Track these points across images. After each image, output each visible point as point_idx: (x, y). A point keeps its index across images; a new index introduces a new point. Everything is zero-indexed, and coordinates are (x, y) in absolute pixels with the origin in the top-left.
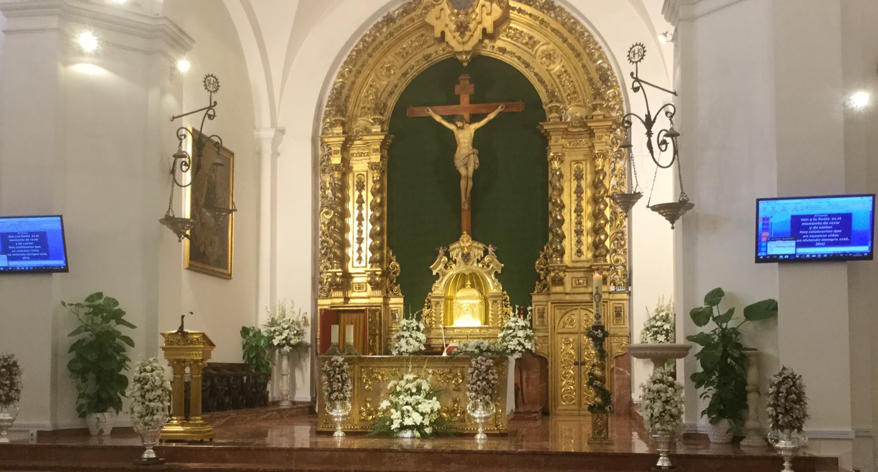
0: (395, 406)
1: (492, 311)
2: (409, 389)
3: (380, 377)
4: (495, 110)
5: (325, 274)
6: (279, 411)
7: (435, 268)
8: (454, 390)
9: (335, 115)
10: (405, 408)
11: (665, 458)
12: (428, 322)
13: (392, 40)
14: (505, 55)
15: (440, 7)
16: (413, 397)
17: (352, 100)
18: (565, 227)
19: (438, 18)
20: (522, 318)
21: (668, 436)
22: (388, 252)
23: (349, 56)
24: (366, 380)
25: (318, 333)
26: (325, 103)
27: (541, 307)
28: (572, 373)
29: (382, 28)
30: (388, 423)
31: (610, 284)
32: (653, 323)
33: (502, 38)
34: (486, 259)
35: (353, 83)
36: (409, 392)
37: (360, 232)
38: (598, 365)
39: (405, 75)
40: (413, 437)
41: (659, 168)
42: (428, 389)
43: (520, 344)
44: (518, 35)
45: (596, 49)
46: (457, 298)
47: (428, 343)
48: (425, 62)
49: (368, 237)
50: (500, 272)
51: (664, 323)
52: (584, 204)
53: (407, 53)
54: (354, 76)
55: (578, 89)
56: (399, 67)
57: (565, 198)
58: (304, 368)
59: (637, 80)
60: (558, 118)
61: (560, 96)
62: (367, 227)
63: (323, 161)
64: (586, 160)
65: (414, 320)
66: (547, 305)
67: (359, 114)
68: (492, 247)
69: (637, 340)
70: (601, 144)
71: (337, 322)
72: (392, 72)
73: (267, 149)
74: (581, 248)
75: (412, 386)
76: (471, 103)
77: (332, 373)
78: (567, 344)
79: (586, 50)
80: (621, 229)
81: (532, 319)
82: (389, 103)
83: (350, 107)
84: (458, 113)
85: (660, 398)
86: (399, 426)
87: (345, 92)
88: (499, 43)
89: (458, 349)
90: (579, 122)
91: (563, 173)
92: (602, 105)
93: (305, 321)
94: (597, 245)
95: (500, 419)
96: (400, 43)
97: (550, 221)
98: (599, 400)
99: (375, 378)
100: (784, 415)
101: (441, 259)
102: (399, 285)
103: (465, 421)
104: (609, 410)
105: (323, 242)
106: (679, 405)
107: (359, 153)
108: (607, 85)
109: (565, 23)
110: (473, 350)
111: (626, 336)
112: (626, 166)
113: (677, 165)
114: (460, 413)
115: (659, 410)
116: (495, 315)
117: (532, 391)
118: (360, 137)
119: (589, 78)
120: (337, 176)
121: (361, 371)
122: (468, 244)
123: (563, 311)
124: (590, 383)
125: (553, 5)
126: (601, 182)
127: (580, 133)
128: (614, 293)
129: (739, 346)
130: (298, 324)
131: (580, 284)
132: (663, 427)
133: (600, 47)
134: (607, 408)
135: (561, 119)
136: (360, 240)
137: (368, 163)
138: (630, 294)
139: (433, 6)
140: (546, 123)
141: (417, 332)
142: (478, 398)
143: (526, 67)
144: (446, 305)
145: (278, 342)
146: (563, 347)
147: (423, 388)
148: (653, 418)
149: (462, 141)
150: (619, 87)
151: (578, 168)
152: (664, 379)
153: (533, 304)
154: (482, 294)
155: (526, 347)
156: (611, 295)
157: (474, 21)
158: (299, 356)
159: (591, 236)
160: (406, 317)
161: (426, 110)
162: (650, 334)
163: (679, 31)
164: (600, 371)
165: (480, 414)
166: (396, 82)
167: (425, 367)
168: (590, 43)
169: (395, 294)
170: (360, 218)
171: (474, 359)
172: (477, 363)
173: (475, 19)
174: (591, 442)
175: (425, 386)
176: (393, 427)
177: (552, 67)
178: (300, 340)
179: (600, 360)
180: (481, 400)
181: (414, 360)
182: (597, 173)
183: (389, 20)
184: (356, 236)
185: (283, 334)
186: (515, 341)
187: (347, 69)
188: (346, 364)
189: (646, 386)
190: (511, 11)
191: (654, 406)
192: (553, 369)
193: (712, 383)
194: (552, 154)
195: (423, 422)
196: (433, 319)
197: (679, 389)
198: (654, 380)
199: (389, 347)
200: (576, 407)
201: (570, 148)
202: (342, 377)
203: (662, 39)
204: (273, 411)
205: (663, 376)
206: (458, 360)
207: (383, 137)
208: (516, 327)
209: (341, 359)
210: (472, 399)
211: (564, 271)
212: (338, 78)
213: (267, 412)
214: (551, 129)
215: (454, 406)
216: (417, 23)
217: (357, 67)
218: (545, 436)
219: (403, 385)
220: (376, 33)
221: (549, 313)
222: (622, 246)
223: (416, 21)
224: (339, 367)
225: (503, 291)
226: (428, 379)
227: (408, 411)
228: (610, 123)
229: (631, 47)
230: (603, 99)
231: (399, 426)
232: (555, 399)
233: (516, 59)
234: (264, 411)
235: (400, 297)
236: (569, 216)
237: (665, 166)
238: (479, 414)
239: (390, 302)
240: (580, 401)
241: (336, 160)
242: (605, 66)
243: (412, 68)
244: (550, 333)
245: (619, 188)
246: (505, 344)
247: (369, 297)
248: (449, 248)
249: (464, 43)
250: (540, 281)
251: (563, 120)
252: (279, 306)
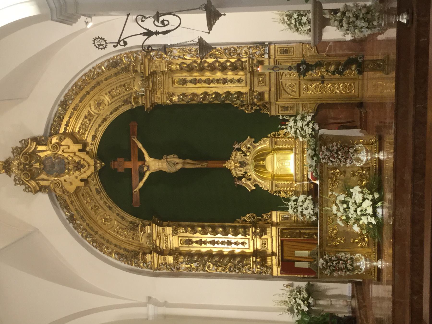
0: (357, 220)
1: (282, 145)
2: (344, 209)
3: (335, 231)
4: (136, 144)
5: (254, 270)
6: (360, 308)
7: (250, 188)
8: (345, 175)
9: (138, 259)
10: (359, 213)
11: (400, 17)
12: (291, 193)
13: (86, 217)
14: (97, 135)
15: (63, 182)
16: (350, 206)
17: (127, 247)
18: (221, 91)
19: (71, 184)
20: (288, 123)
21: (383, 15)
22: (238, 223)
23: (96, 248)
24: (337, 242)
25: (299, 276)
26: (130, 266)
27: (280, 109)
28: (330, 85)
29: (77, 224)
30: (371, 226)
31: (263, 58)
32: (292, 26)
33: (86, 138)
34: (244, 149)
35: (116, 246)
36: (346, 209)
37: (223, 243)
38: (327, 68)
39: (110, 208)
40: (382, 207)
41: (180, 26)
42: (344, 195)
43: (308, 125)
44: (84, 127)
45: (95, 70)
46: (273, 171)
47: (307, 194)
48: (101, 193)
49: (227, 237)
50: (253, 140)
51: (293, 18)
52: (203, 78)
53: (95, 206)
54: (111, 245)
55: (122, 83)
56: (105, 212)
57: (199, 91)
58: (326, 287)
59: (118, 43)
60: (142, 97)
61: (127, 96)
62: (219, 237)
63: (171, 269)
64: (172, 77)
65: (289, 204)
66: (278, 105)
67: (138, 242)
68: (235, 145)
69: (308, 38)
70: (161, 66)
71: (293, 262)
72: (108, 217)
73: (162, 310)
74: (236, 79)
75: (342, 207)
76: (130, 160)
77: (332, 268)
78: (307, 89)
79: (95, 77)
80: (222, 51)
81: (288, 116)
82: (130, 220)
83: (132, 248)
84: (138, 170)
85: (354, 22)
86: (374, 218)
87: (122, 252)
88: (89, 140)
89: (313, 172)
90: (145, 82)
91: (181, 93)
92: (133, 66)
93: (289, 286)
94: (235, 68)
95: (368, 141)
96: (88, 212)
97: (216, 102)
98: (354, 67)
99: (335, 235)
101: (243, 183)
102: (263, 214)
103: (369, 168)
104: (362, 59)
105: (230, 271)
106: (360, 7)
107: (165, 243)
108: (120, 62)
109: (76, 92)
110: (314, 161)
111: (302, 46)
112: (177, 48)
113: (178, 12)
114: (363, 171)
115: (363, 23)
116: (286, 143)
117: (343, 116)
118: (154, 241)
119: (114, 76)
120: (182, 259)
121: (330, 246)
122: (233, 163)
123: (283, 92)
125: (63, 101)
126: (188, 66)
127: (153, 82)
128: (270, 55)
130: (292, 291)
131: (262, 80)
132: (376, 19)
133: (93, 68)
134: (360, 60)
135: (143, 95)
136: (229, 243)
137: (173, 236)
138: (270, 43)
139: (62, 187)
140: (146, 106)
141: (298, 201)
142: (352, 158)
143: (106, 121)
144: (278, 180)
145: (306, 307)
146: (310, 92)
147: (343, 199)
148: (369, 27)
150: (121, 54)
151: (178, 82)
152: (339, 19)
153: (278, 114)
154: (269, 153)
155: (310, 120)
156: (271, 57)
157: (74, 158)
158: (317, 291)
159: (228, 72)
160: (287, 209)
161: (135, 193)
162: (301, 27)
163: (84, 13)
164: (331, 66)
165: (363, 156)
166: (115, 214)
167: (327, 197)
168: (90, 75)
169: (270, 218)
170: (213, 243)
171: (321, 160)
172: (324, 158)
173: (72, 157)
174: (386, 73)
175: (342, 197)
176: (374, 222)
177: (106, 102)
178: (304, 290)
179: (323, 66)
180: (353, 155)
181: (322, 205)
182: (182, 69)
183: (72, 219)
184: (226, 246)
185: (299, 303)
186: (306, 128)
187: (106, 250)
188: (324, 257)
189: (345, 32)
190: (67, 132)
191: (360, 26)
192: (327, 100)
194: (168, 102)
195: (370, 199)
196: (288, 189)
197: (347, 8)
198: (339, 27)
199: (310, 223)
200: (357, 83)
201: (164, 89)
202: (335, 261)
203: (90, 25)
204: (360, 313)
205: (337, 20)
206: (322, 172)
207: (154, 225)
208: (295, 127)
209: (321, 261)
210: (352, 162)
211: (253, 92)
212: (112, 257)
213: (361, 318)
214: (150, 102)
215: (358, 176)
216: (74, 198)
217: (104, 242)
218: (381, 105)
219: (341, 214)
220: (80, 228)
221: (285, 103)
222: (235, 49)
223: (73, 200)
224: (327, 263)
225: (267, 137)
226: (336, 195)
227: (362, 211)
228: (146, 60)
229: (95, 47)
230: (129, 65)
231: (374, 218)
232: (350, 98)
233: (100, 128)
234: (360, 320)
235: (272, 214)
236: (213, 89)
237: (179, 19)
238: (364, 157)
239: (275, 221)
240: (352, 79)
241: (170, 259)
242: (106, 64)
243: (105, 203)
244: (299, 102)
245: (193, 53)
246: (307, 136)
247: (272, 237)
248: (235, 177)
249: (89, 165)
250: (261, 109)
251: (144, 94)
252: (278, 305)
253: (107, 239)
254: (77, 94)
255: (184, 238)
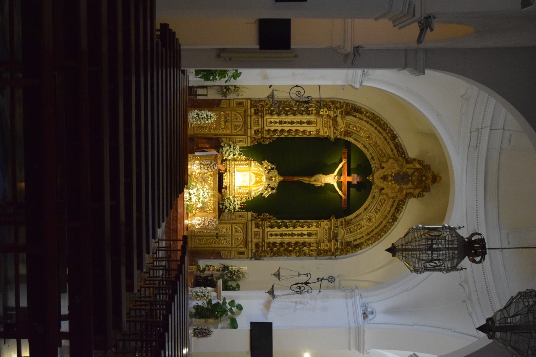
29: (391, 134)
43: (226, 207)
50: (263, 195)
59: (321, 280)
65: (239, 152)
72: (368, 139)
100: (198, 332)
102: (257, 143)
124: (207, 266)
129: (222, 316)
136: (281, 123)
149: (328, 178)
153: (246, 212)
165: (196, 222)
193: (208, 306)
225: (253, 197)
235: (251, 144)
242: (363, 247)
250: (258, 216)
253: (368, 124)
254: (385, 226)
255: (312, 125)
